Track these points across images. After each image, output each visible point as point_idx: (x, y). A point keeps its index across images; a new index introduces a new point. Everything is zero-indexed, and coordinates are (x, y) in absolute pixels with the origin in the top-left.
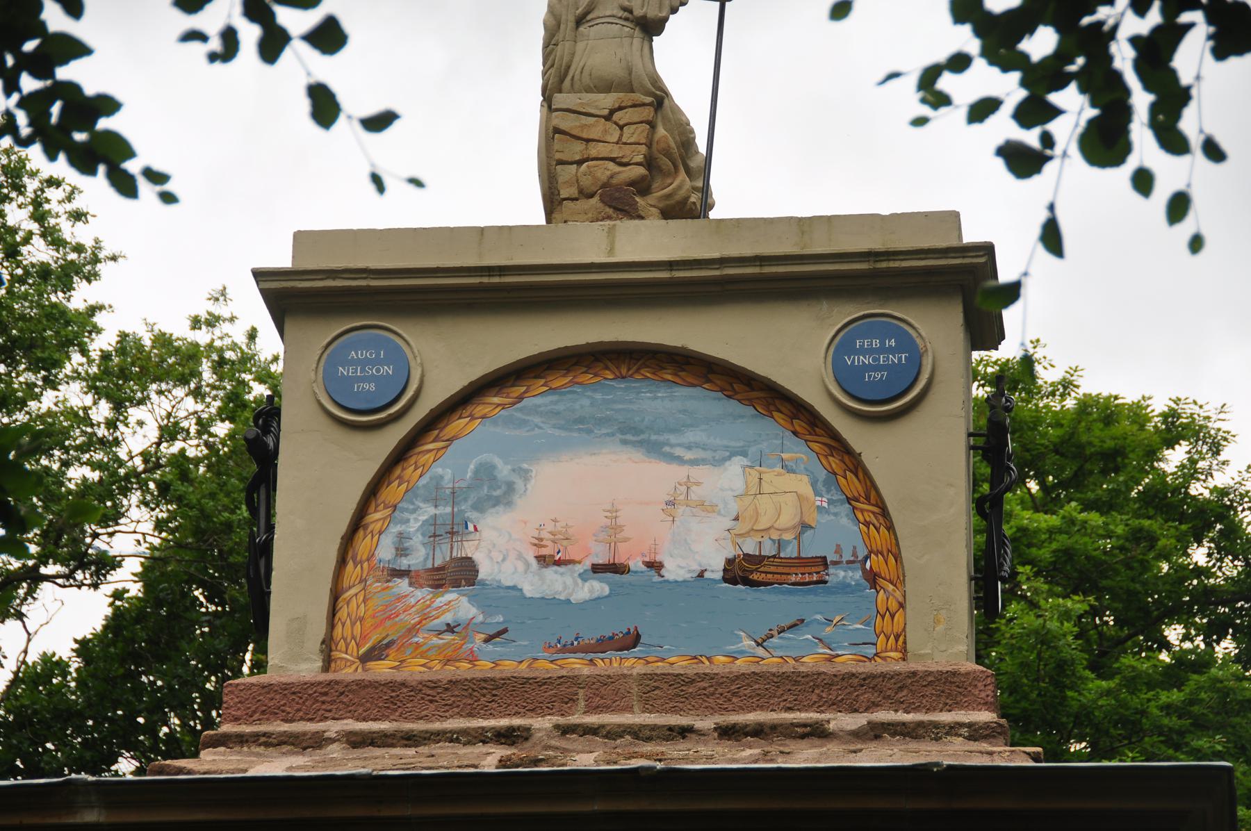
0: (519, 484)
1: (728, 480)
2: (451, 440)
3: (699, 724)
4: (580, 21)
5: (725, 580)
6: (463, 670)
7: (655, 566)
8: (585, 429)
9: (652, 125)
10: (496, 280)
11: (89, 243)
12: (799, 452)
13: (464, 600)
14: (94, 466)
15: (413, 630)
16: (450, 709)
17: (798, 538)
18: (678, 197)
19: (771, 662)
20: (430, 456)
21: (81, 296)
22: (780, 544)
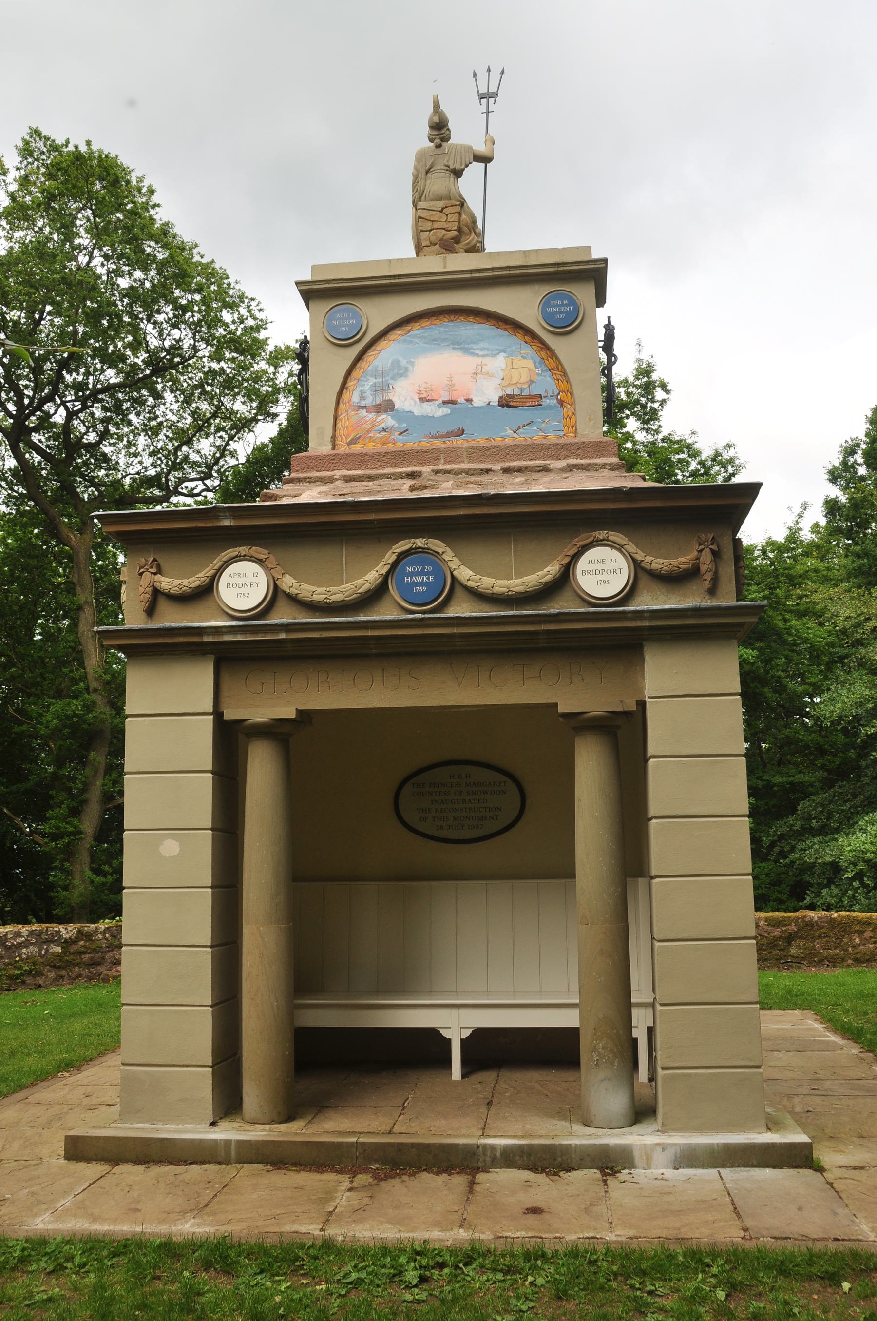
0: (410, 368)
1: (498, 363)
2: (381, 350)
3: (493, 468)
4: (427, 172)
5: (499, 405)
6: (390, 447)
7: (469, 400)
8: (436, 343)
9: (460, 214)
10: (397, 281)
11: (264, 318)
12: (528, 350)
13: (389, 417)
14: (270, 386)
15: (369, 431)
16: (386, 464)
17: (529, 386)
18: (472, 244)
19: (520, 438)
20: (372, 358)
21: (262, 335)
22: (522, 390)
